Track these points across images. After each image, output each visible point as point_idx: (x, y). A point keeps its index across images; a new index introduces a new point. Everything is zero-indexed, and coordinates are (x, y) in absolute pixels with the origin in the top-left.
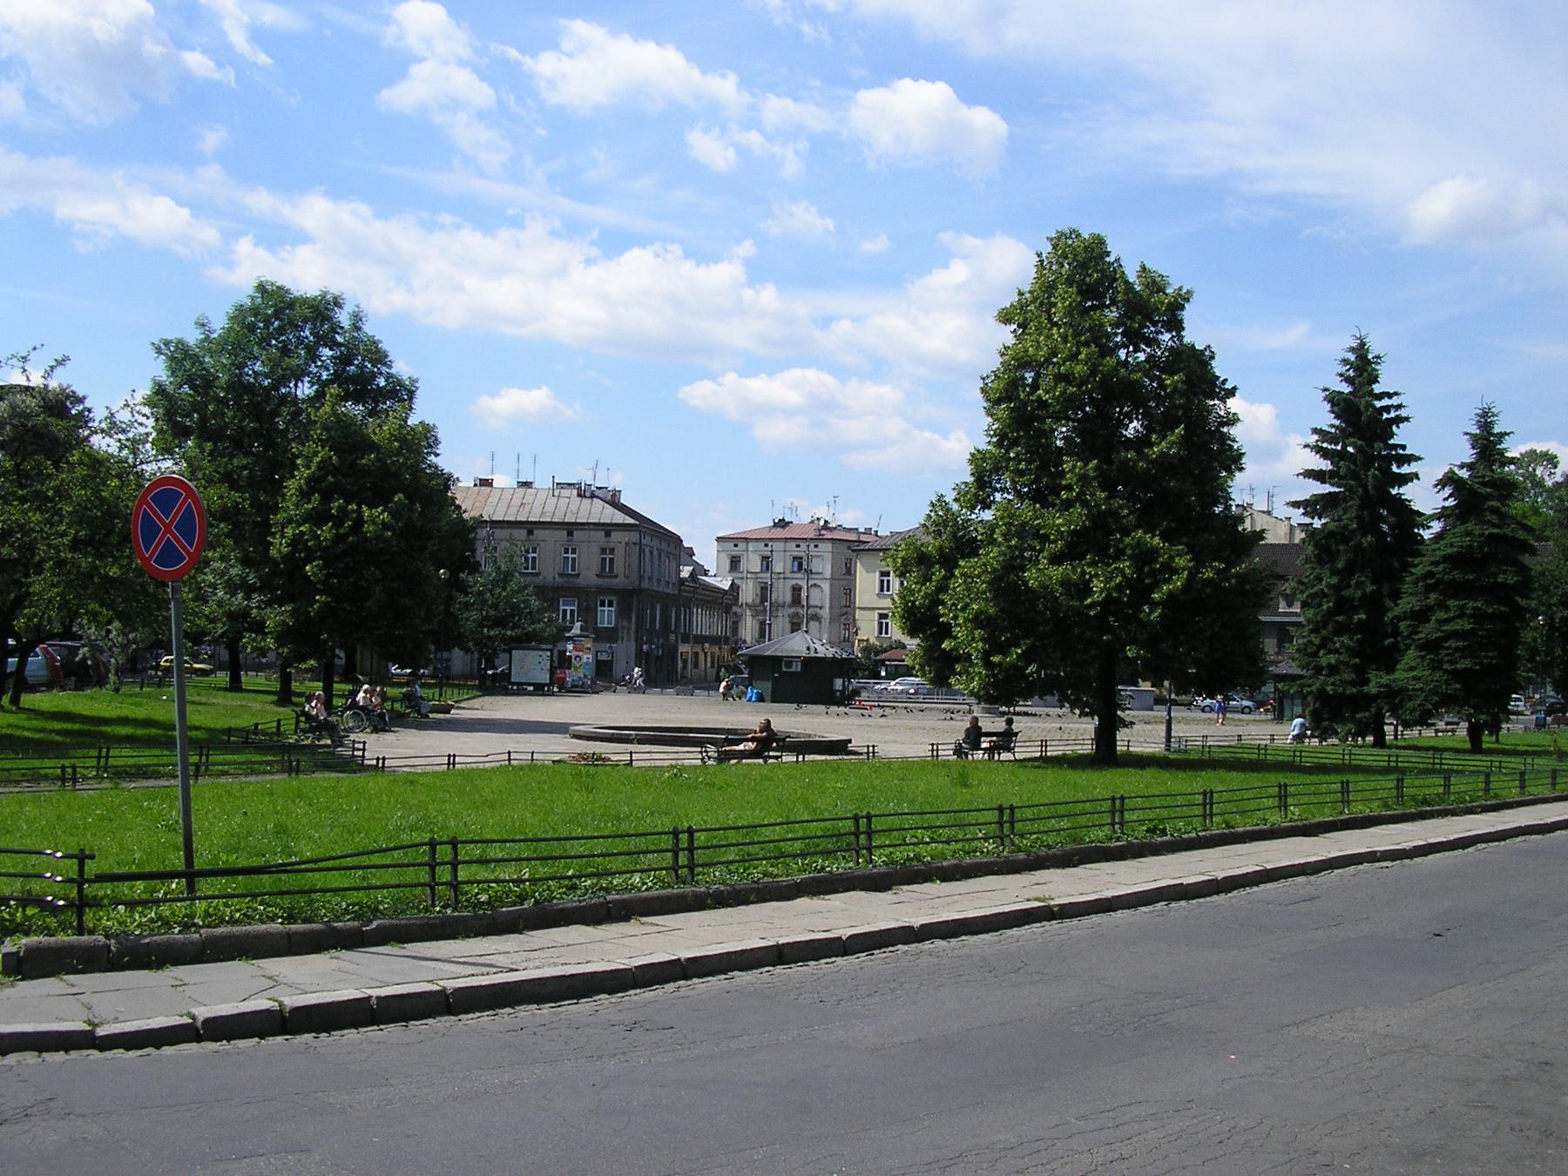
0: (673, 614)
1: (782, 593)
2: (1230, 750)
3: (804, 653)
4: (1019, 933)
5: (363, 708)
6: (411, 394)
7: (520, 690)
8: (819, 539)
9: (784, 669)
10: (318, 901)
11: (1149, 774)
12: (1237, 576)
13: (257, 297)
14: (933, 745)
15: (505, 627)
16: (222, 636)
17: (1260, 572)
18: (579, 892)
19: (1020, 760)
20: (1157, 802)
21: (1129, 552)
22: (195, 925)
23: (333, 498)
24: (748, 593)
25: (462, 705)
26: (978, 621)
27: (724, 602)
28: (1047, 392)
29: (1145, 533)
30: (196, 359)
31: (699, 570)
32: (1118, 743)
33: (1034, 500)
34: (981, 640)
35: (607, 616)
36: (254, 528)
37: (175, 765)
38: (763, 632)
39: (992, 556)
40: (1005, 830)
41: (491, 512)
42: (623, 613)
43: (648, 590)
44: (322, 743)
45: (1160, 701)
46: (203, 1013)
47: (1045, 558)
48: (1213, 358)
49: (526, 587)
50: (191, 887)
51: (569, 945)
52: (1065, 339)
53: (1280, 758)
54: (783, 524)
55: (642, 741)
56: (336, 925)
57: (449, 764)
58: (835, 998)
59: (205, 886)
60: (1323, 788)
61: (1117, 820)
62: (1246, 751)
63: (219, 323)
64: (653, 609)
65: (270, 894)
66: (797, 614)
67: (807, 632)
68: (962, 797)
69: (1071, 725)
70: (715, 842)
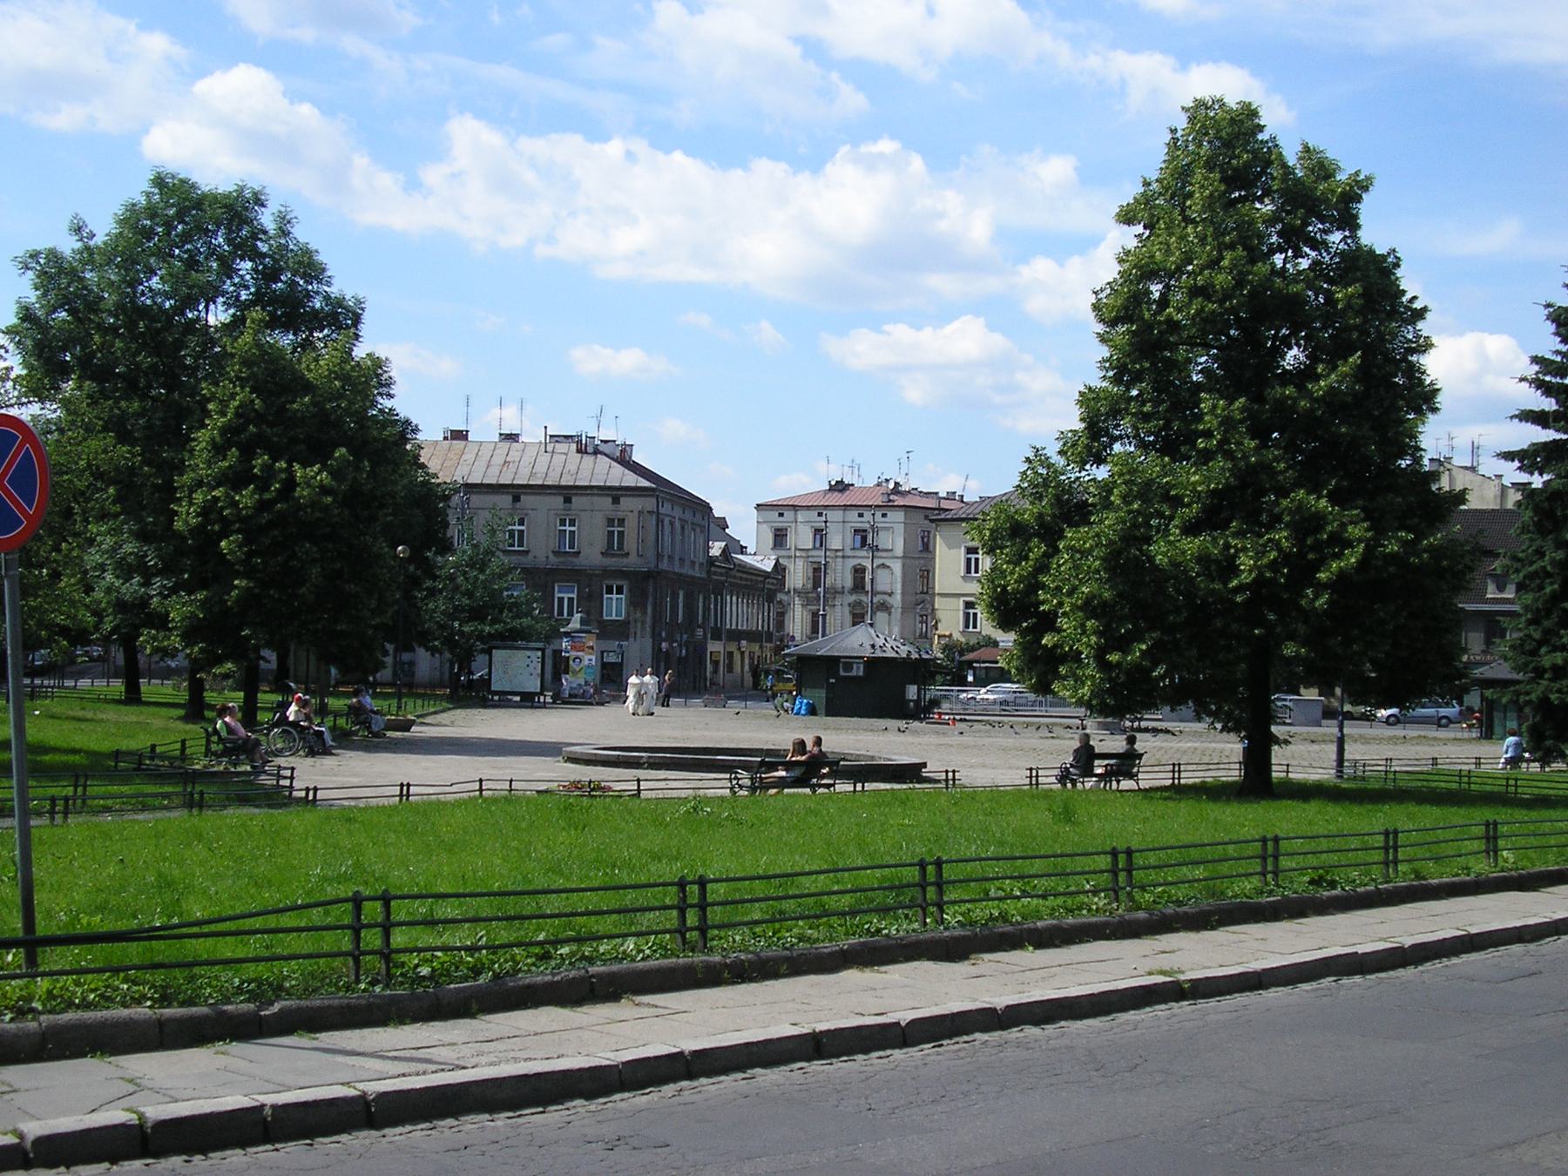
0: (701, 605)
1: (840, 575)
2: (1422, 777)
3: (868, 652)
4: (1138, 1018)
5: (295, 724)
6: (357, 319)
7: (502, 700)
8: (888, 506)
9: (842, 673)
10: (201, 976)
11: (1312, 808)
12: (1431, 549)
13: (154, 194)
14: (1031, 769)
15: (483, 620)
16: (114, 630)
17: (1462, 545)
18: (553, 963)
19: (1146, 790)
20: (1324, 844)
21: (1287, 519)
22: (33, 1010)
23: (256, 453)
24: (797, 576)
25: (428, 720)
26: (1090, 608)
27: (766, 587)
28: (1179, 310)
29: (1309, 493)
30: (74, 274)
31: (734, 546)
32: (1274, 768)
33: (1163, 452)
34: (1094, 633)
35: (615, 606)
36: (153, 494)
37: (12, 800)
38: (816, 626)
39: (1108, 524)
40: (1120, 879)
41: (465, 473)
42: (636, 602)
43: (667, 572)
44: (239, 769)
45: (1329, 714)
46: (34, 1129)
47: (1176, 527)
48: (1399, 266)
49: (511, 570)
50: (32, 960)
51: (536, 1034)
52: (1203, 240)
53: (1488, 788)
54: (840, 488)
55: (654, 765)
56: (225, 1008)
57: (401, 795)
58: (888, 1105)
59: (54, 958)
60: (1547, 827)
61: (1270, 868)
62: (1442, 778)
63: (103, 228)
64: (675, 597)
65: (137, 968)
66: (859, 604)
67: (871, 625)
68: (1070, 837)
69: (1213, 745)
70: (737, 897)
